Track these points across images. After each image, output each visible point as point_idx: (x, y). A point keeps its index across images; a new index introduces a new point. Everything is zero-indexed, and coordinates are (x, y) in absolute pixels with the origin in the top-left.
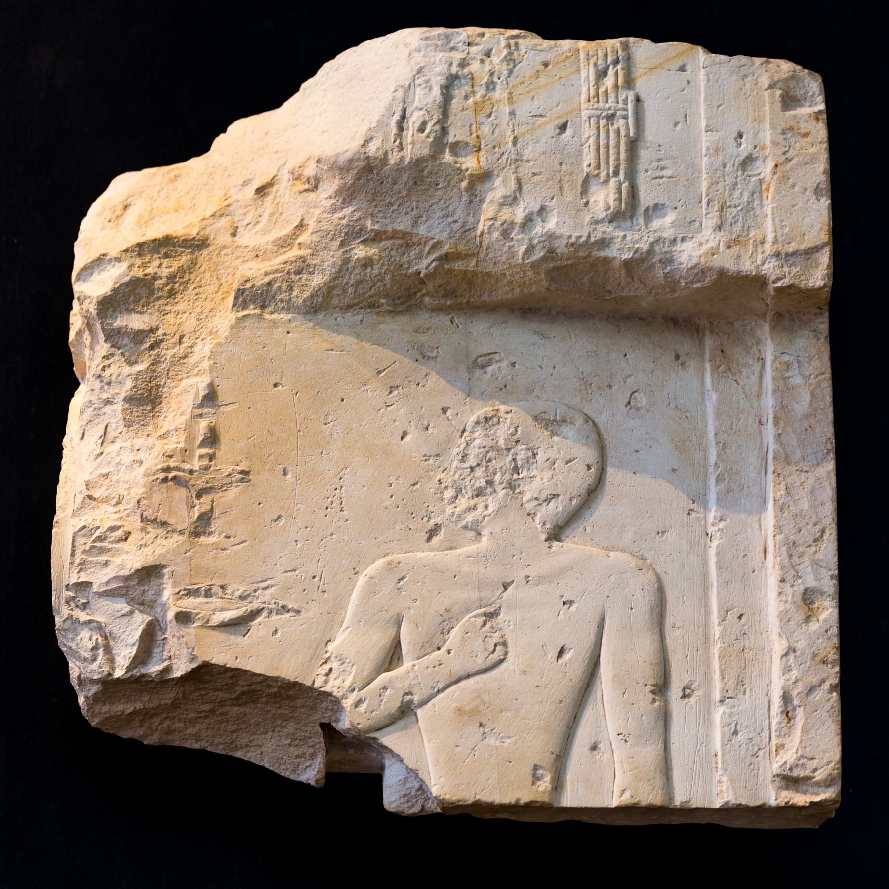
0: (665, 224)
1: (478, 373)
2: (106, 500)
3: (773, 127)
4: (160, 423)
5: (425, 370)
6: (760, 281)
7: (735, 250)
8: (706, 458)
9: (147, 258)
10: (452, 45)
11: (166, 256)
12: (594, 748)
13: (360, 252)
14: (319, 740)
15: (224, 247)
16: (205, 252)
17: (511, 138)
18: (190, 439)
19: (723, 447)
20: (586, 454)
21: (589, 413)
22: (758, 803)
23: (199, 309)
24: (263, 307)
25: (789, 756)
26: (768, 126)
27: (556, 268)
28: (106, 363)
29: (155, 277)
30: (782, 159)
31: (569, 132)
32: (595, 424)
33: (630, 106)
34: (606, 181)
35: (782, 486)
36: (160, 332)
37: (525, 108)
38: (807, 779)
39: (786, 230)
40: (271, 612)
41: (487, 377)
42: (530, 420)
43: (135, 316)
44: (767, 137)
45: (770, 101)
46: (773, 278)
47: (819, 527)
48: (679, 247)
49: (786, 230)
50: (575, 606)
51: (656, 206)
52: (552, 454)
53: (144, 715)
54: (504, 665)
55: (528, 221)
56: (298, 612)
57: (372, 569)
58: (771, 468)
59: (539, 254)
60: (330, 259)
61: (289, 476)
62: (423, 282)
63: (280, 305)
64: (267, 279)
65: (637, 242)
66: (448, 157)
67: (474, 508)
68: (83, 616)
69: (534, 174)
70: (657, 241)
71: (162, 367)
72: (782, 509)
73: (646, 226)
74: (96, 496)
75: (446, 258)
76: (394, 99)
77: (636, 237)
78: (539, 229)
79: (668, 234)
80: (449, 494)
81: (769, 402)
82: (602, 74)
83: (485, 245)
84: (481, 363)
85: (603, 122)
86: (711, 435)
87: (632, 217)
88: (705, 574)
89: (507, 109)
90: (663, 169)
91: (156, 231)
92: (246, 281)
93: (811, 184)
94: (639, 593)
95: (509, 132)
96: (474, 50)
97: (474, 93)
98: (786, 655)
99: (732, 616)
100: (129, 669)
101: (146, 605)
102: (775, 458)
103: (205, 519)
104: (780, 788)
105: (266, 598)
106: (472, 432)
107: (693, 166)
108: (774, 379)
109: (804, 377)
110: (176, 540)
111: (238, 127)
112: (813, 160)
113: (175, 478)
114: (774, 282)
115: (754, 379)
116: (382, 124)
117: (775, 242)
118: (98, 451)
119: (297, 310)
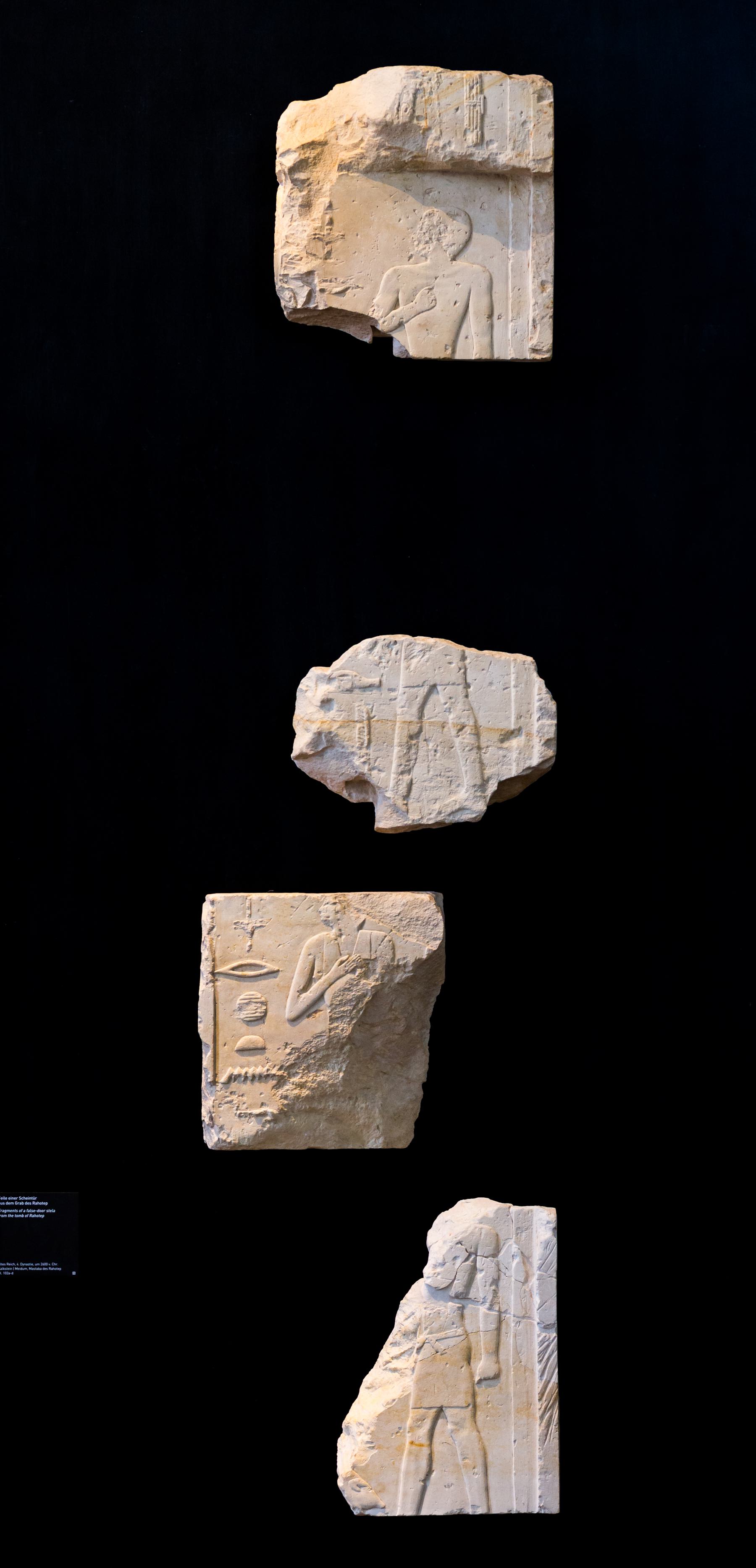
0: (494, 147)
1: (427, 196)
2: (293, 243)
3: (534, 110)
4: (312, 215)
5: (407, 195)
6: (528, 170)
7: (519, 158)
8: (508, 228)
9: (305, 150)
10: (417, 76)
11: (313, 149)
12: (467, 338)
13: (383, 153)
14: (370, 330)
15: (333, 145)
16: (327, 147)
17: (438, 114)
18: (323, 223)
19: (515, 225)
20: (465, 228)
21: (467, 212)
22: (524, 358)
23: (325, 170)
24: (348, 171)
25: (534, 342)
26: (532, 109)
27: (454, 163)
28: (292, 191)
29: (309, 158)
30: (537, 123)
31: (459, 111)
32: (468, 215)
33: (482, 101)
34: (473, 131)
35: (535, 242)
36: (311, 180)
37: (443, 102)
38: (540, 350)
39: (537, 151)
40: (353, 288)
41: (430, 197)
42: (445, 214)
43: (302, 174)
44: (532, 113)
45: (533, 98)
46: (532, 169)
47: (547, 258)
48: (499, 156)
49: (537, 151)
50: (460, 286)
51: (491, 140)
52: (453, 228)
53: (307, 318)
54: (435, 308)
55: (444, 146)
56: (362, 288)
57: (389, 271)
58: (531, 235)
59: (448, 159)
60: (373, 155)
61: (359, 236)
62: (406, 163)
63: (355, 170)
64: (349, 161)
65: (484, 154)
66: (415, 122)
67: (425, 248)
68: (286, 286)
69: (447, 128)
70: (491, 154)
71: (312, 193)
72: (534, 251)
73: (487, 148)
74: (289, 241)
75: (415, 157)
76: (396, 98)
77: (483, 152)
78: (448, 149)
79: (495, 151)
80: (416, 243)
81: (531, 209)
82: (472, 88)
83: (429, 153)
84: (427, 192)
85: (472, 108)
86: (511, 220)
87: (482, 145)
88: (507, 273)
89: (437, 103)
90: (493, 125)
91: (308, 139)
92: (342, 161)
93: (547, 133)
94: (483, 281)
95: (438, 111)
96: (425, 78)
97: (425, 96)
98: (534, 305)
99: (516, 289)
100: (303, 306)
101: (308, 284)
102: (533, 231)
103: (329, 253)
104: (531, 353)
105: (351, 283)
106: (424, 219)
107: (505, 125)
108: (533, 201)
109: (544, 200)
110: (319, 261)
111: (338, 87)
112: (548, 123)
113: (318, 238)
114: (533, 170)
115: (527, 198)
116: (391, 108)
117: (533, 155)
118: (290, 224)
119: (361, 172)
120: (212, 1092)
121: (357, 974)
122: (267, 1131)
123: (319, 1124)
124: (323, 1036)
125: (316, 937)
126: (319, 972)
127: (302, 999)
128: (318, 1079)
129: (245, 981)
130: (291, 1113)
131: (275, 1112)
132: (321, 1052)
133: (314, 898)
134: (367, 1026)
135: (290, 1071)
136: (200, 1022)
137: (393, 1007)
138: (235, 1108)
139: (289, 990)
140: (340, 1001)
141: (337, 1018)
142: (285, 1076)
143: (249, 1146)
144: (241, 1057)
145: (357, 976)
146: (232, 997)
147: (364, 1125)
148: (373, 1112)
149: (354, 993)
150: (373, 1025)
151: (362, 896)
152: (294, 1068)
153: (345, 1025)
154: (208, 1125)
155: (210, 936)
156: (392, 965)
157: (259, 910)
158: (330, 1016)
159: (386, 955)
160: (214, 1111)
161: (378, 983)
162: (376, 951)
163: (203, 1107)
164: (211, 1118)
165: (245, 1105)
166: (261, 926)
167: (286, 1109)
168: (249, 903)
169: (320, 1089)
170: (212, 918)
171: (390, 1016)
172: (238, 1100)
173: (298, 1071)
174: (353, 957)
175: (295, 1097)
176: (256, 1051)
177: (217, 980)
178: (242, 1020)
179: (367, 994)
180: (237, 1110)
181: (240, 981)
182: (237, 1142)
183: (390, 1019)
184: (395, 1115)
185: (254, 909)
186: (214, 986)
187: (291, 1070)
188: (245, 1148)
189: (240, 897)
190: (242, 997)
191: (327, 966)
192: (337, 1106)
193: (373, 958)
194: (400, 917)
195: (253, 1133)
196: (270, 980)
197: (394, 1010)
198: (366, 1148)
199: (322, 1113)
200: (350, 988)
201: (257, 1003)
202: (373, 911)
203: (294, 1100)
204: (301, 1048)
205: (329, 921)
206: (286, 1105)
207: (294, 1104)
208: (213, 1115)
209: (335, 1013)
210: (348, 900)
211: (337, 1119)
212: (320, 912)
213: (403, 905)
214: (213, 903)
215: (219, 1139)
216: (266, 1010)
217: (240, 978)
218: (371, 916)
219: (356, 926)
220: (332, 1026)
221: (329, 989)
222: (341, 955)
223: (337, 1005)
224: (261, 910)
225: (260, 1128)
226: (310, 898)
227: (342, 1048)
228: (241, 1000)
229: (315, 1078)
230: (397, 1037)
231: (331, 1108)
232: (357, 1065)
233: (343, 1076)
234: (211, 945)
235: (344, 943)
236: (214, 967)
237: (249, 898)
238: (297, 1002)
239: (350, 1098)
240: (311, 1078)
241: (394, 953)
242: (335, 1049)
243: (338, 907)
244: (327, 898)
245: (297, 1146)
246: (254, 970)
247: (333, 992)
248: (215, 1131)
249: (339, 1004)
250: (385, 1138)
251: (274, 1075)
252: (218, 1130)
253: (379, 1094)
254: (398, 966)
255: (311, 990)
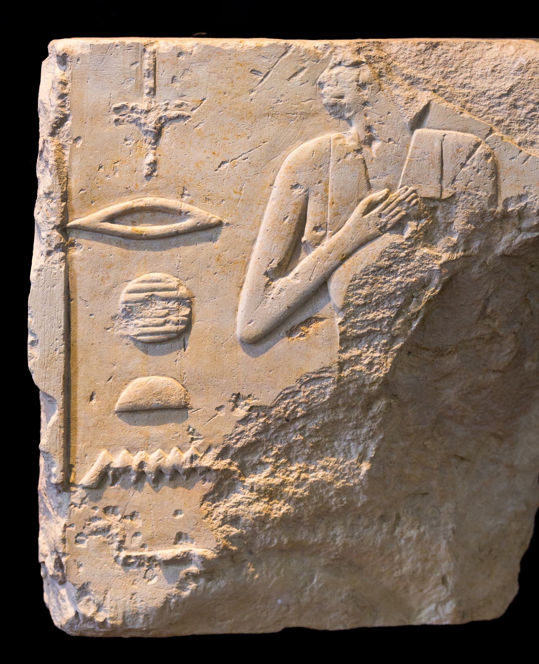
120: (60, 505)
121: (407, 233)
122: (191, 598)
123: (312, 578)
124: (323, 378)
125: (311, 144)
126: (316, 229)
127: (275, 291)
128: (312, 478)
129: (138, 249)
130: (246, 556)
131: (210, 554)
132: (320, 416)
133: (307, 51)
134: (426, 355)
135: (246, 459)
136: (33, 343)
137: (489, 310)
138: (115, 545)
139: (245, 272)
140: (366, 297)
141: (359, 337)
142: (234, 472)
143: (148, 631)
144: (128, 426)
145: (408, 239)
146: (108, 284)
147: (413, 575)
148: (433, 548)
149: (398, 279)
150: (440, 352)
151: (422, 47)
152: (255, 452)
153: (377, 354)
154: (52, 576)
155: (56, 141)
156: (492, 213)
157: (173, 79)
158: (343, 333)
159: (477, 189)
160: (67, 550)
161: (455, 256)
162: (454, 180)
163: (41, 532)
164: (59, 564)
165: (139, 538)
166: (179, 117)
167: (234, 548)
168: (151, 61)
169: (315, 499)
170: (62, 96)
171: (481, 331)
172: (121, 526)
173: (263, 458)
174: (399, 193)
175: (256, 519)
176: (166, 413)
177: (72, 244)
178: (134, 340)
179: (430, 281)
180: (119, 549)
181: (127, 247)
182: (119, 622)
183: (480, 338)
184: (481, 550)
185: (163, 76)
186: (64, 258)
187: (248, 458)
188: (138, 635)
189: (130, 47)
190: (131, 286)
191: (336, 214)
192: (352, 536)
193: (445, 195)
194: (511, 99)
195: (158, 601)
196: (199, 246)
197: (489, 316)
198: (415, 623)
199: (319, 552)
200: (390, 266)
201: (167, 299)
202: (447, 83)
203: (253, 526)
204: (271, 408)
205: (342, 106)
206: (234, 537)
207: (254, 534)
208: (64, 560)
209: (353, 326)
210: (389, 55)
211: (351, 564)
212: (321, 85)
213: (520, 69)
214: (63, 59)
215: (77, 613)
216: (190, 316)
217: (127, 241)
218: (442, 95)
219: (407, 120)
220: (346, 356)
221: (341, 268)
222: (369, 187)
223: (358, 306)
224: (178, 78)
225: (174, 591)
226: (298, 49)
227: (368, 406)
228: (130, 292)
229: (303, 475)
230: (493, 377)
231: (339, 541)
232: (401, 444)
233: (368, 471)
234: (59, 162)
235: (378, 160)
236: (66, 214)
237: (150, 49)
238: (264, 298)
239: (383, 518)
240: (295, 475)
241: (496, 186)
242: (350, 408)
243: (366, 73)
244: (337, 51)
245: (259, 626)
246: (162, 222)
247: (351, 277)
248: (68, 591)
249: (365, 305)
250: (459, 604)
251: (208, 470)
252: (74, 593)
253: (449, 506)
254: (506, 216)
255: (296, 270)
